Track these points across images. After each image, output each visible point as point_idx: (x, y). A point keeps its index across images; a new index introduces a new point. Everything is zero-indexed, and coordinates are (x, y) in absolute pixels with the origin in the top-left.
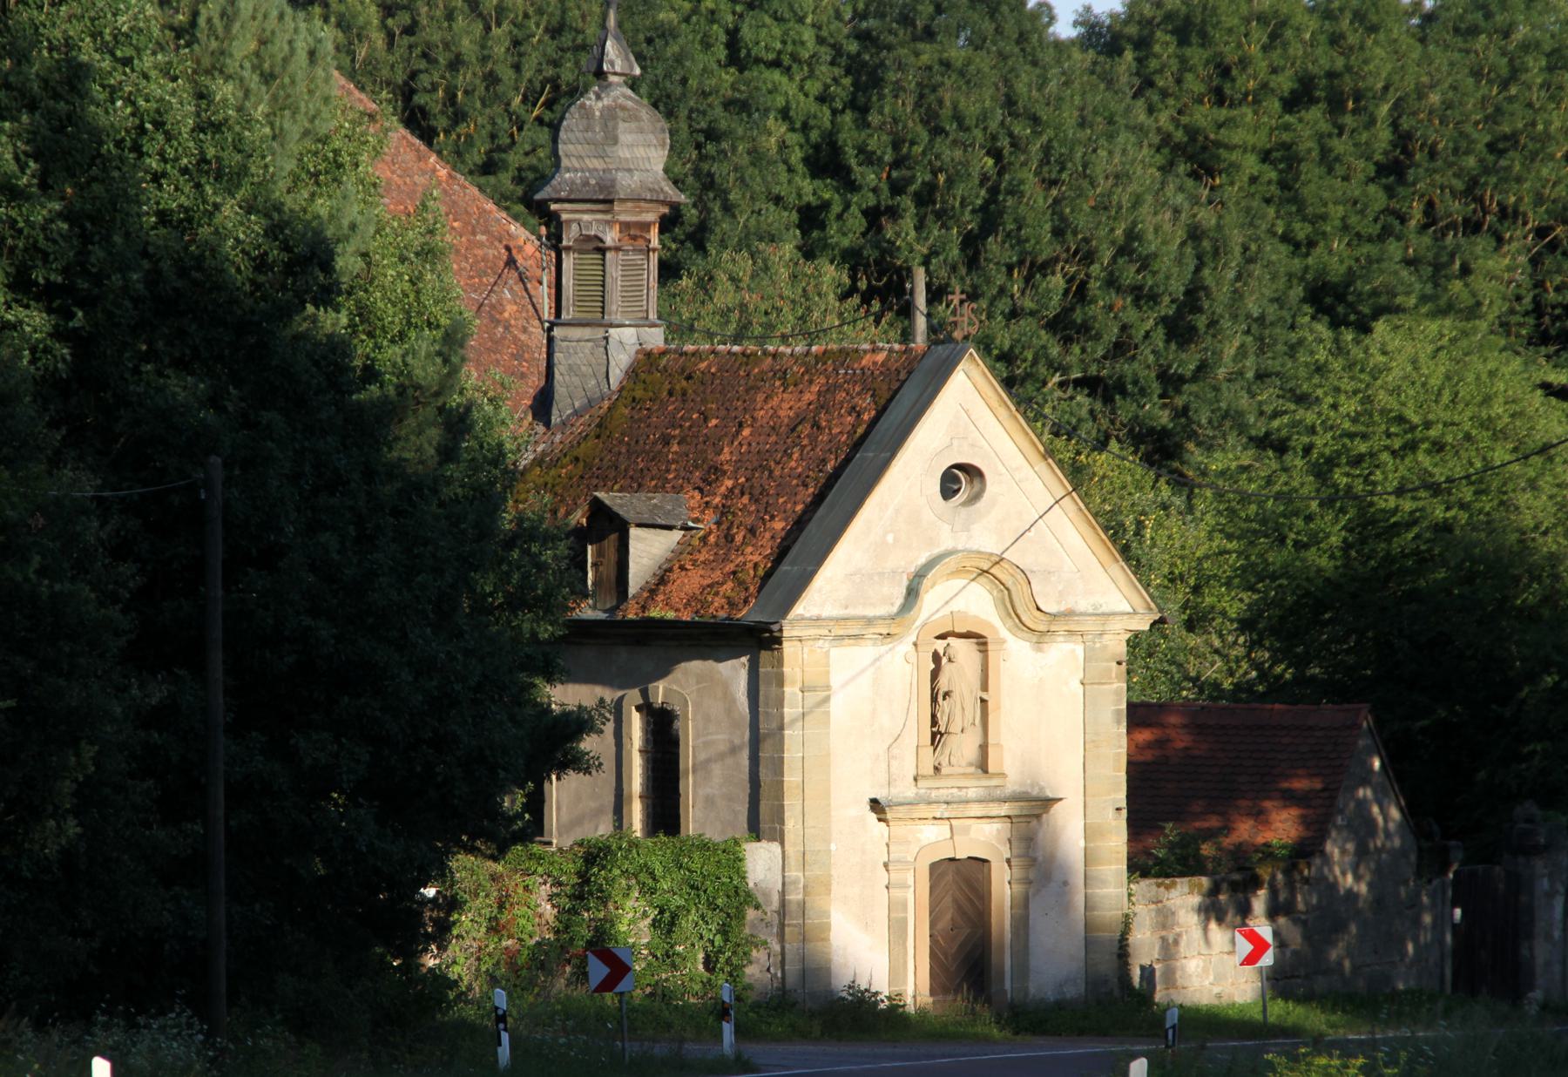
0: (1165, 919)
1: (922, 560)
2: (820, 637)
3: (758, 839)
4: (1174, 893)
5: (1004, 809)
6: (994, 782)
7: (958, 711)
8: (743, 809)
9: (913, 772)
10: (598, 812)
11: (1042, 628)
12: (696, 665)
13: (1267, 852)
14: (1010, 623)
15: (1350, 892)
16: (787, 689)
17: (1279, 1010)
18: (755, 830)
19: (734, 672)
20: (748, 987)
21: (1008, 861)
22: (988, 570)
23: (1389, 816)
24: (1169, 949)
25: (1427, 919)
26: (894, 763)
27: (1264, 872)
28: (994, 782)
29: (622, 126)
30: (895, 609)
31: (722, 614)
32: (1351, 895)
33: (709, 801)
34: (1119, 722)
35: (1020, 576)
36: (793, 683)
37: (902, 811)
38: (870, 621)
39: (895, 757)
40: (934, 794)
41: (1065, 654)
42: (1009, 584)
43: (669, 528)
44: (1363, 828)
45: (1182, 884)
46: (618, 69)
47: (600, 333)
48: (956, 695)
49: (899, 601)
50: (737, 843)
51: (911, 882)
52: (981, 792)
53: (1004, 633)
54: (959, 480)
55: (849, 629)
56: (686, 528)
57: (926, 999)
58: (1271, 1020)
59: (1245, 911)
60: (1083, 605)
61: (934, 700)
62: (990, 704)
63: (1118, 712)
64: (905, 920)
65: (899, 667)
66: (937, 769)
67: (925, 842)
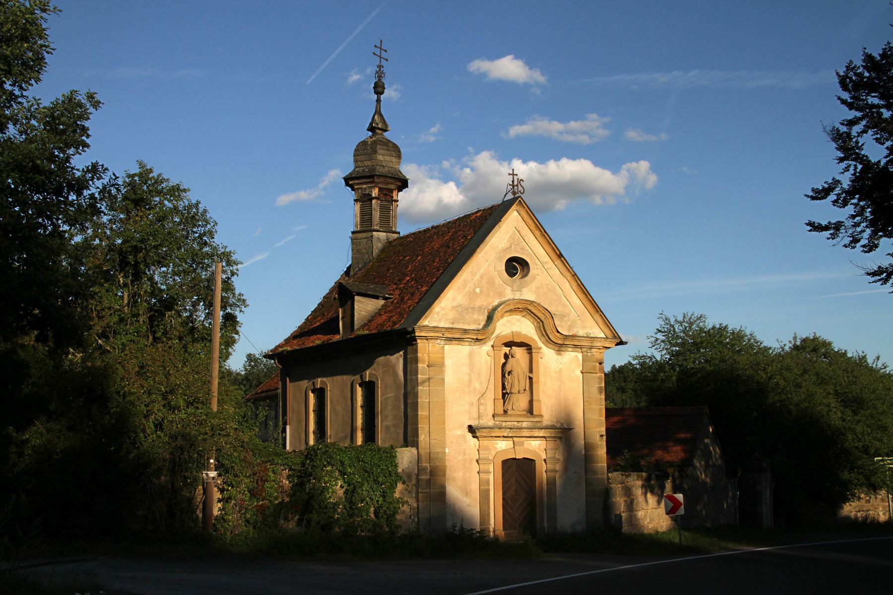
0: (628, 492)
1: (496, 303)
2: (437, 338)
3: (407, 446)
4: (630, 479)
5: (541, 433)
6: (536, 419)
7: (516, 382)
8: (401, 431)
9: (491, 413)
10: (345, 438)
11: (560, 342)
12: (382, 358)
13: (671, 464)
14: (544, 339)
15: (704, 481)
16: (420, 365)
17: (687, 538)
18: (406, 444)
19: (397, 360)
20: (399, 527)
21: (545, 460)
22: (526, 309)
23: (716, 451)
24: (631, 505)
25: (730, 494)
26: (482, 408)
27: (670, 470)
28: (536, 419)
29: (379, 146)
30: (481, 327)
31: (389, 329)
32: (704, 482)
33: (387, 428)
34: (601, 393)
35: (548, 315)
36: (423, 362)
37: (484, 433)
38: (465, 331)
39: (482, 404)
40: (504, 424)
41: (572, 359)
42: (543, 319)
43: (377, 297)
44: (707, 455)
45: (634, 475)
46: (380, 126)
47: (369, 234)
48: (515, 373)
49: (483, 323)
50: (392, 447)
51: (491, 470)
52: (529, 424)
53: (541, 344)
54: (516, 266)
55: (455, 336)
56: (385, 298)
57: (500, 532)
58: (684, 543)
59: (662, 488)
60: (581, 333)
61: (503, 376)
62: (534, 380)
63: (600, 388)
64: (488, 490)
65: (485, 356)
66: (505, 412)
67: (499, 449)
